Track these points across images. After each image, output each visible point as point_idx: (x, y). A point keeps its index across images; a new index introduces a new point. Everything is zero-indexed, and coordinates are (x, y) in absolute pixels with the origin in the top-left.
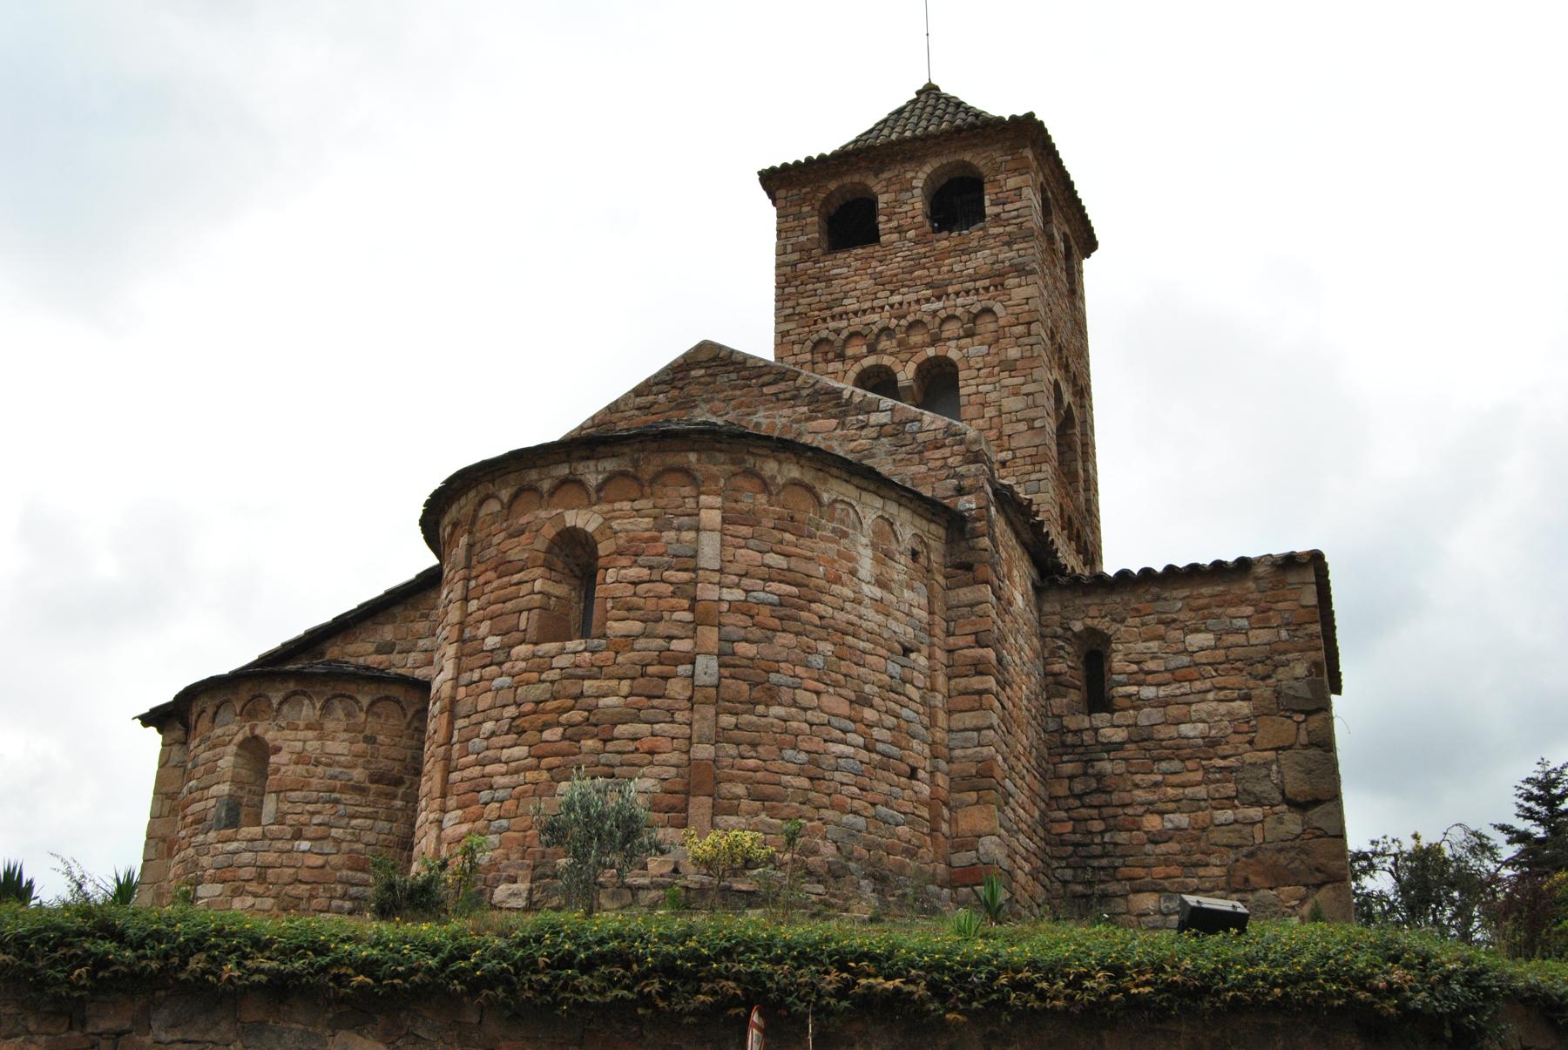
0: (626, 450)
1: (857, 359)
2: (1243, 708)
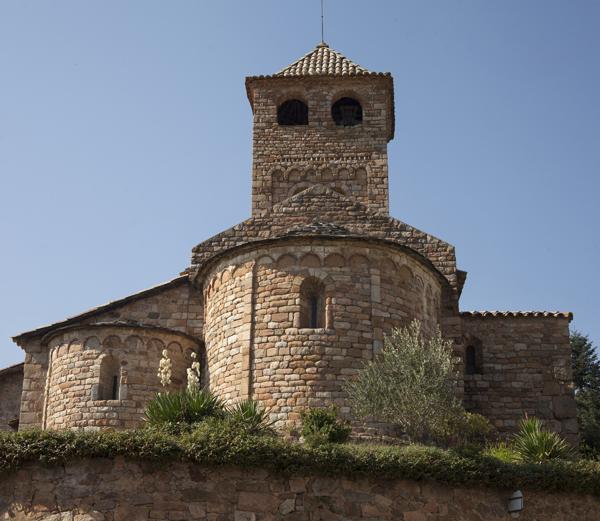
0: (338, 243)
1: (295, 183)
2: (539, 377)
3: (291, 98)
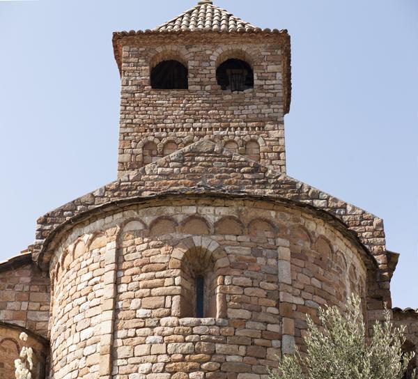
0: (234, 203)
3: (166, 58)
